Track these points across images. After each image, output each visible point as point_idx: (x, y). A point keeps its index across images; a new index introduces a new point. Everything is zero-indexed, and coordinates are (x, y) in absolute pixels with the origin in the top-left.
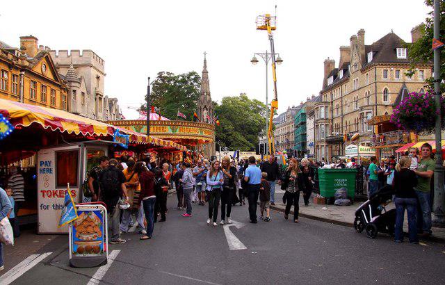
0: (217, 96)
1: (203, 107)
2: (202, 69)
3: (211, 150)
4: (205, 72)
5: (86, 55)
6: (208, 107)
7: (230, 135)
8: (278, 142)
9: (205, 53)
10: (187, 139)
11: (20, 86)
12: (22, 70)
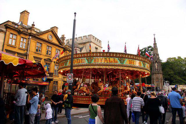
0: (164, 59)
1: (155, 62)
2: (153, 43)
3: (161, 85)
4: (155, 44)
5: (89, 37)
6: (158, 61)
7: (172, 77)
9: (154, 35)
10: (134, 71)
11: (28, 44)
12: (30, 36)
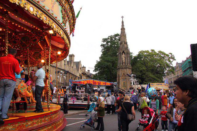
0: (134, 51)
1: (121, 52)
8: (171, 81)
9: (122, 17)
